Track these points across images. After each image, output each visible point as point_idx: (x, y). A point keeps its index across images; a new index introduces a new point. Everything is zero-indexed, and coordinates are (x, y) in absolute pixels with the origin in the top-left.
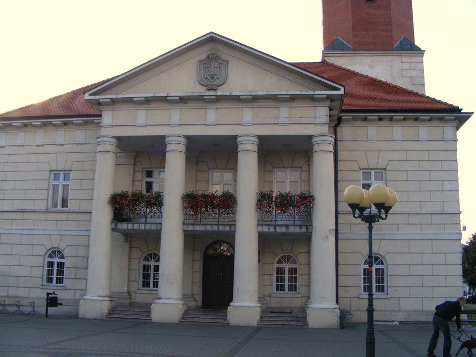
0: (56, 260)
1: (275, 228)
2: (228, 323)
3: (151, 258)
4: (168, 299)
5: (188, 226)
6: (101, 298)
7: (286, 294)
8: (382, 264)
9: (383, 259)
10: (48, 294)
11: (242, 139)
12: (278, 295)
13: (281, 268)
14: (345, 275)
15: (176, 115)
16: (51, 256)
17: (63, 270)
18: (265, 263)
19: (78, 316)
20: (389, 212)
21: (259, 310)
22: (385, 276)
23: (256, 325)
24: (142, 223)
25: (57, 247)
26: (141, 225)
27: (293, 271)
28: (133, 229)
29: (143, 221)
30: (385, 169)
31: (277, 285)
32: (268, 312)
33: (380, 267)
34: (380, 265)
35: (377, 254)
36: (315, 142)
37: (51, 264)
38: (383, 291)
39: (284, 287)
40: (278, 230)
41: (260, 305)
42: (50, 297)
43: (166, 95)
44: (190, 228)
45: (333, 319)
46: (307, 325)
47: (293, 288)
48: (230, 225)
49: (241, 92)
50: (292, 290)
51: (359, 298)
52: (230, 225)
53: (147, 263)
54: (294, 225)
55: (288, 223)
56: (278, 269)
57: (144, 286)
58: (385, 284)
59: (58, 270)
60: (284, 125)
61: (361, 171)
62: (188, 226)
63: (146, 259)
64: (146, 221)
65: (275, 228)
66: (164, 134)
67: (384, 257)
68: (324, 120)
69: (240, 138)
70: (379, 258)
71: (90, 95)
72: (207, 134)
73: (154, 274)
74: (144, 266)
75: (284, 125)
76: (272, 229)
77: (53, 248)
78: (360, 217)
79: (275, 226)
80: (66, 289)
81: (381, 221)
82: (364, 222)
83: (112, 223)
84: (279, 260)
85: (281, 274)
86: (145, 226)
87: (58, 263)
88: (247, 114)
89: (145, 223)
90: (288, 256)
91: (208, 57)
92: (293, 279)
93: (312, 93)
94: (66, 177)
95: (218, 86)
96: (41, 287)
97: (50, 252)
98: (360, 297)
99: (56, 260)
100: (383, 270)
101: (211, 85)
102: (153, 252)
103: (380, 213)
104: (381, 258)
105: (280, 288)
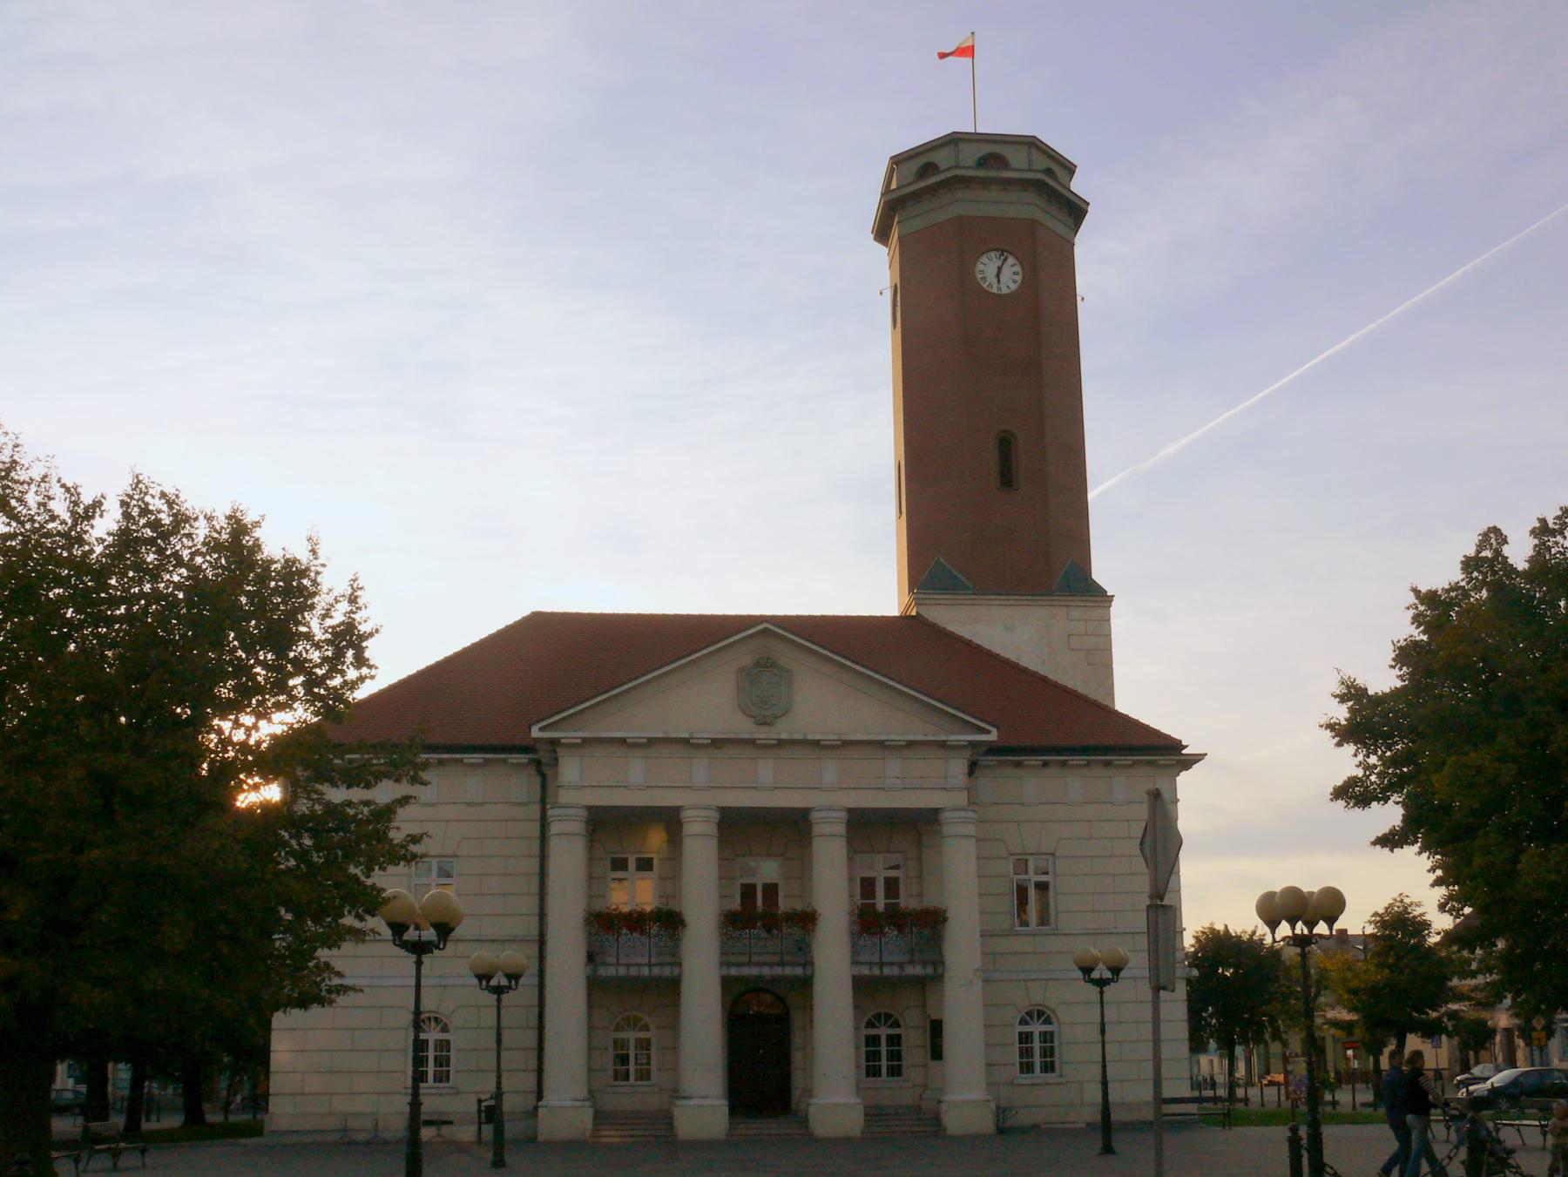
1: (881, 969)
2: (812, 1134)
4: (703, 1097)
6: (579, 1103)
7: (430, 1088)
8: (899, 1026)
9: (1052, 1015)
10: (480, 1101)
11: (823, 814)
13: (622, 1040)
15: (700, 769)
17: (1020, 1043)
19: (536, 1138)
20: (449, 939)
21: (861, 1109)
22: (1056, 1044)
24: (610, 965)
25: (436, 1009)
26: (642, 967)
27: (895, 1040)
28: (1101, 978)
29: (612, 960)
30: (1053, 854)
32: (873, 1114)
33: (642, 1035)
34: (1047, 1026)
35: (1041, 1005)
36: (816, 819)
37: (1025, 1038)
38: (1053, 1070)
39: (435, 1076)
40: (887, 971)
41: (860, 1101)
42: (486, 1107)
43: (687, 736)
44: (733, 971)
45: (984, 1122)
46: (945, 1130)
47: (895, 1071)
50: (441, 1081)
51: (1012, 1083)
52: (804, 965)
53: (621, 1035)
54: (911, 962)
55: (639, 960)
56: (1020, 1034)
58: (1056, 1059)
60: (891, 789)
61: (1011, 857)
62: (772, 967)
63: (618, 1028)
65: (881, 969)
66: (680, 804)
67: (1054, 1012)
69: (948, 813)
70: (1044, 1013)
71: (541, 729)
73: (636, 1055)
74: (867, 1038)
75: (891, 789)
76: (876, 971)
79: (881, 965)
80: (457, 1094)
81: (436, 952)
82: (410, 954)
85: (1027, 1042)
88: (830, 770)
89: (618, 964)
91: (758, 664)
92: (895, 1056)
93: (944, 738)
95: (776, 718)
98: (1015, 1082)
99: (1036, 1028)
100: (1052, 1033)
101: (764, 717)
104: (1048, 1012)
105: (1027, 1068)
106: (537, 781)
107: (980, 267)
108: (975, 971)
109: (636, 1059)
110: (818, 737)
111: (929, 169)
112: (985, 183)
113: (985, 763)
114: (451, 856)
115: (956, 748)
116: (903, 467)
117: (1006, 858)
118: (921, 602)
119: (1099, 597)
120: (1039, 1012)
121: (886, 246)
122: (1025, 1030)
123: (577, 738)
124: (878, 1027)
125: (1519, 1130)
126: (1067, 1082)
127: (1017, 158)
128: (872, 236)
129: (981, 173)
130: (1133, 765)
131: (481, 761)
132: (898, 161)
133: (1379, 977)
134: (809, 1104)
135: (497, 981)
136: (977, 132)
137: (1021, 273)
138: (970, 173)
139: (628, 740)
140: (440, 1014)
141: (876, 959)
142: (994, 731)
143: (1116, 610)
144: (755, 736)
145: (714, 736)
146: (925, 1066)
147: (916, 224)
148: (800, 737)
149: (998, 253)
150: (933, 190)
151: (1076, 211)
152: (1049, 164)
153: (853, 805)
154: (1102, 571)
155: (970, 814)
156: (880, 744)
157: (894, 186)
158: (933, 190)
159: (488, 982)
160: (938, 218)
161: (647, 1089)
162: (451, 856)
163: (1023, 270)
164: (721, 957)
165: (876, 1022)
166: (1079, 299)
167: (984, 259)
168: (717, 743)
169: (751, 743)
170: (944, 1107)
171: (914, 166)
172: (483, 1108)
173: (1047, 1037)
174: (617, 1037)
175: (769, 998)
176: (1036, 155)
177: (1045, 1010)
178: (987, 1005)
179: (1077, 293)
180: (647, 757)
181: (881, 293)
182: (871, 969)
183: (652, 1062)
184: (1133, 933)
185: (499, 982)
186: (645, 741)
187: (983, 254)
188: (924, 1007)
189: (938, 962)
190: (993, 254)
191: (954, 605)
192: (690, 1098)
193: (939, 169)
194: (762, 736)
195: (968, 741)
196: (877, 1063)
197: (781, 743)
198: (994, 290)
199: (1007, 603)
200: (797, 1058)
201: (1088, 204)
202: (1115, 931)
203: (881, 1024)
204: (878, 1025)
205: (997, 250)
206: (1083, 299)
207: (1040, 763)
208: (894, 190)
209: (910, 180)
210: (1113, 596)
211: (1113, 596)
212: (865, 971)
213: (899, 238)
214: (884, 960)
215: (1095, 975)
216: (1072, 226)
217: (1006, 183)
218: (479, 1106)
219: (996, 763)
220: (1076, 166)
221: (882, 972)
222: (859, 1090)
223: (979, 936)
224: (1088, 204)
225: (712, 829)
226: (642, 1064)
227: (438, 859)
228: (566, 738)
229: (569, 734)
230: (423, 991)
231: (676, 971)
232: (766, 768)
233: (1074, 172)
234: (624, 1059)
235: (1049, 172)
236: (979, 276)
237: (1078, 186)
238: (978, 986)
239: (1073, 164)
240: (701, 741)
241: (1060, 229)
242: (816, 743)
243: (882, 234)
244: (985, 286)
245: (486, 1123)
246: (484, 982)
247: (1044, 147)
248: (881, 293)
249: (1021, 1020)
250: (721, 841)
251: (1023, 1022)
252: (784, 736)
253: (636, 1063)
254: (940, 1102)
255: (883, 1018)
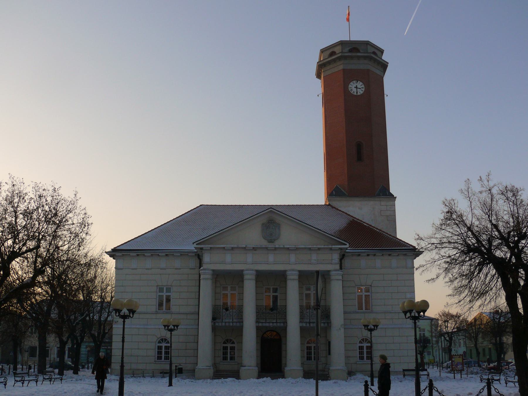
0: (164, 345)
1: (310, 324)
3: (163, 342)
5: (259, 323)
6: (207, 368)
11: (290, 272)
12: (361, 363)
13: (309, 347)
14: (411, 349)
15: (249, 257)
16: (159, 342)
18: (220, 343)
23: (312, 379)
31: (307, 357)
37: (160, 348)
41: (302, 368)
42: (178, 368)
43: (245, 246)
47: (232, 358)
48: (240, 322)
49: (309, 245)
50: (166, 359)
51: (356, 363)
53: (309, 345)
56: (307, 347)
57: (223, 360)
59: (165, 351)
62: (259, 323)
63: (224, 343)
64: (222, 321)
65: (310, 324)
68: (337, 262)
71: (197, 244)
72: (231, 269)
73: (230, 352)
74: (223, 347)
77: (161, 337)
78: (119, 316)
79: (310, 323)
83: (212, 322)
84: (308, 342)
86: (233, 324)
87: (165, 346)
90: (365, 338)
94: (169, 290)
95: (274, 240)
96: (154, 362)
97: (159, 339)
98: (304, 363)
99: (229, 345)
101: (271, 240)
102: (233, 340)
103: (130, 314)
105: (225, 358)
106: (198, 261)
107: (350, 86)
108: (341, 325)
109: (230, 353)
110: (288, 247)
111: (333, 53)
112: (352, 58)
113: (347, 255)
114: (170, 286)
115: (335, 250)
116: (325, 154)
117: (355, 287)
118: (330, 200)
119: (392, 198)
120: (161, 339)
121: (320, 79)
122: (360, 345)
123: (251, 247)
124: (363, 343)
125: (514, 384)
126: (375, 363)
127: (338, 50)
128: (316, 76)
129: (350, 54)
130: (398, 255)
131: (121, 255)
132: (322, 51)
133: (3, 329)
134: (240, 369)
135: (370, 327)
136: (351, 40)
137: (364, 87)
138: (346, 54)
139: (311, 248)
140: (166, 337)
141: (308, 321)
142: (348, 244)
143: (397, 202)
144: (267, 246)
145: (254, 246)
146: (327, 357)
147: (329, 72)
148: (282, 246)
149: (356, 81)
150: (334, 61)
151: (384, 66)
152: (373, 50)
153: (257, 269)
154: (392, 190)
155: (340, 272)
156: (310, 249)
157: (322, 59)
158: (334, 61)
159: (367, 327)
160: (336, 70)
161: (233, 363)
162: (170, 286)
163: (365, 86)
164: (256, 320)
165: (363, 342)
166: (385, 96)
167: (351, 83)
168: (254, 249)
169: (267, 248)
170: (330, 371)
171: (328, 52)
172: (177, 369)
173: (232, 348)
174: (224, 346)
175: (275, 333)
176: (369, 47)
177: (162, 338)
178: (345, 337)
179: (385, 93)
180: (274, 254)
181: (318, 96)
182: (306, 324)
183: (235, 354)
184: (399, 313)
185: (371, 327)
186: (209, 248)
187: (351, 82)
188: (326, 337)
189: (285, 323)
190: (354, 82)
191: (349, 201)
192: (245, 366)
193: (336, 53)
194: (270, 246)
195: (339, 248)
196: (165, 355)
197: (276, 249)
198: (355, 94)
199: (359, 200)
200: (283, 353)
201: (388, 63)
202: (392, 312)
203: (364, 342)
204: (227, 343)
205: (356, 80)
206: (387, 96)
207: (366, 255)
208: (322, 60)
209: (327, 57)
210: (396, 197)
211: (396, 197)
212: (304, 325)
213: (323, 77)
214: (311, 321)
215: (369, 327)
216: (383, 71)
217: (359, 58)
218: (176, 368)
219: (351, 255)
220: (384, 50)
221: (310, 325)
222: (303, 364)
223: (343, 314)
224: (388, 63)
225: (254, 277)
226: (232, 355)
227: (166, 287)
228: (205, 247)
229: (206, 246)
230: (125, 330)
231: (241, 324)
232: (271, 258)
233: (383, 52)
234: (166, 353)
235: (374, 53)
236: (350, 89)
237: (385, 57)
238: (342, 330)
239: (383, 50)
240: (250, 248)
241: (378, 72)
242: (288, 249)
243: (318, 76)
244: (352, 92)
245: (178, 373)
246: (166, 327)
247: (372, 45)
248: (318, 96)
249: (360, 342)
250: (257, 281)
251: (360, 342)
252: (277, 246)
253: (230, 355)
254: (329, 369)
255: (161, 341)
